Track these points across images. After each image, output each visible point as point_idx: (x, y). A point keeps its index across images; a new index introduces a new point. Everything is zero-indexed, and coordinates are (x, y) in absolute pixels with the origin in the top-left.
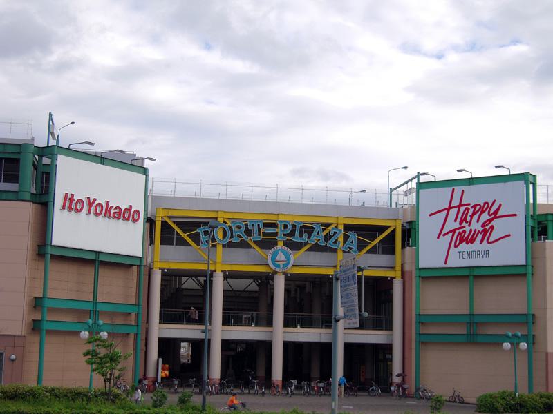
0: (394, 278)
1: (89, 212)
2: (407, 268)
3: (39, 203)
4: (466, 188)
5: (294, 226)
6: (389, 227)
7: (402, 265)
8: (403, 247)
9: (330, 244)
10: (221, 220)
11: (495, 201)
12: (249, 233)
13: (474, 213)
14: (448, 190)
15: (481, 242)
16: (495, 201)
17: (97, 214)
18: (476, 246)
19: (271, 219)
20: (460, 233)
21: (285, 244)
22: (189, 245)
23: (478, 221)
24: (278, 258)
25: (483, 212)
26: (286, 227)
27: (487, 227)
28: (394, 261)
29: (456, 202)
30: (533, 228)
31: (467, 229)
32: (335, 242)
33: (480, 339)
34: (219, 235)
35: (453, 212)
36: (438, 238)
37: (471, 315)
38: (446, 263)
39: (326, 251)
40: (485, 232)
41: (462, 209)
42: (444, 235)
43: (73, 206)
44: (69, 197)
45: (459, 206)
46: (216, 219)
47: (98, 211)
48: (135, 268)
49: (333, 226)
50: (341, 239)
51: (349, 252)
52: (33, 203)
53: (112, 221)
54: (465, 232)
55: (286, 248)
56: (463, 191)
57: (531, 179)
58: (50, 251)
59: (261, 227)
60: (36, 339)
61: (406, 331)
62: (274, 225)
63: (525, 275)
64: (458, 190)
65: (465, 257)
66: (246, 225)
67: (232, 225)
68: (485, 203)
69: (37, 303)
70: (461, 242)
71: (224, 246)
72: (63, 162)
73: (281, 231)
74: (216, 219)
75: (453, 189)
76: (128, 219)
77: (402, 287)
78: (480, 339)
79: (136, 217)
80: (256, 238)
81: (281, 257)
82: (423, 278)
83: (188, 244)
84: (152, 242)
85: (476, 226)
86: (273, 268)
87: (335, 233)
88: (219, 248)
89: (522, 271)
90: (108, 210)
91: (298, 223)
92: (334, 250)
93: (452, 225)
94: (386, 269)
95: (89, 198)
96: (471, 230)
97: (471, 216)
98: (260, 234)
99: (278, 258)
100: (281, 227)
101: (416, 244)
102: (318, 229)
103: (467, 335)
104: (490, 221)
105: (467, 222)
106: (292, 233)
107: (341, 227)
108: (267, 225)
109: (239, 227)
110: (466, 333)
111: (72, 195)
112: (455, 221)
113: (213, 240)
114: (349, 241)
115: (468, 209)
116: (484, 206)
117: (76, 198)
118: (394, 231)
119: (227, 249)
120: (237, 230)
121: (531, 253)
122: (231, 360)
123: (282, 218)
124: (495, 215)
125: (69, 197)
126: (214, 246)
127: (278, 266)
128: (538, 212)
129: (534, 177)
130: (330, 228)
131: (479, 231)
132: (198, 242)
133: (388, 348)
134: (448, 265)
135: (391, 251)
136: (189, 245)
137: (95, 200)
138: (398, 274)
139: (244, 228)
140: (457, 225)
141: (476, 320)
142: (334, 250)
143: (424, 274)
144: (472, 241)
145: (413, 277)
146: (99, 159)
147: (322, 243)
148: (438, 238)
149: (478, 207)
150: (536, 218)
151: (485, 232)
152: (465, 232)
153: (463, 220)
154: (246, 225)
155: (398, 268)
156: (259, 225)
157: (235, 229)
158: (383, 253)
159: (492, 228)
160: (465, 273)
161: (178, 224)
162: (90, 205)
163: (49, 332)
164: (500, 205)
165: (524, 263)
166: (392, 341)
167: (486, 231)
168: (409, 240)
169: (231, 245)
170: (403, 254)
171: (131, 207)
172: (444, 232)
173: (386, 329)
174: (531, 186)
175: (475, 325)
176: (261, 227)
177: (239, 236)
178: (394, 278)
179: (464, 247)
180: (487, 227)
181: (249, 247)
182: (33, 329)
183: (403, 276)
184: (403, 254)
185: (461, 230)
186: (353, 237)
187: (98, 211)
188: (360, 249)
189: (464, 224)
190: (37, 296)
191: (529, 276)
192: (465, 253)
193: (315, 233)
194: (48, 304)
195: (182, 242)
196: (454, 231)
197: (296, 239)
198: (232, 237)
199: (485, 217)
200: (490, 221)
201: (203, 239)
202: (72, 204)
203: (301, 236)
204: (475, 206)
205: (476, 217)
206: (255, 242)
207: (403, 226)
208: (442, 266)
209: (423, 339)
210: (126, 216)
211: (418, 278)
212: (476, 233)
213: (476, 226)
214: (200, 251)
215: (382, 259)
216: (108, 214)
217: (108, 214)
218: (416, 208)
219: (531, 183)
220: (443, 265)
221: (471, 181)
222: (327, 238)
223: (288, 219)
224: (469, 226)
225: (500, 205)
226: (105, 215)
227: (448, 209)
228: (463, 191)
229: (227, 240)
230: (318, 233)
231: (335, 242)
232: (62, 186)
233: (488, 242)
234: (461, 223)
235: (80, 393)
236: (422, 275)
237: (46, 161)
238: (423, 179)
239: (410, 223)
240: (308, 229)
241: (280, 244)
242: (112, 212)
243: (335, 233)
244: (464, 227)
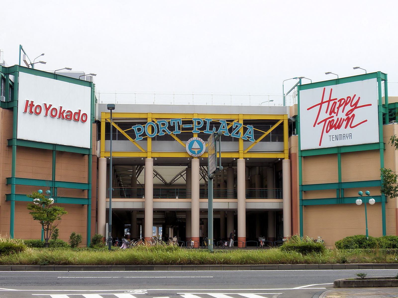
0: (284, 159)
1: (46, 115)
2: (293, 151)
3: (8, 109)
4: (333, 87)
5: (205, 123)
6: (278, 120)
7: (290, 150)
8: (290, 134)
9: (233, 135)
10: (149, 120)
11: (355, 95)
12: (171, 128)
13: (340, 106)
14: (321, 89)
15: (346, 128)
16: (355, 95)
17: (53, 116)
18: (342, 130)
19: (189, 117)
20: (330, 122)
21: (199, 136)
22: (127, 139)
23: (343, 112)
24: (193, 147)
25: (346, 104)
26: (199, 123)
27: (350, 116)
28: (283, 147)
29: (326, 98)
30: (384, 115)
31: (335, 118)
32: (237, 133)
33: (346, 201)
34: (149, 131)
35: (325, 106)
36: (314, 126)
37: (340, 183)
38: (320, 145)
39: (232, 141)
40: (348, 119)
41: (332, 103)
42: (318, 124)
44: (30, 103)
45: (330, 100)
46: (147, 119)
47: (54, 114)
48: (86, 156)
49: (236, 121)
50: (241, 131)
51: (248, 140)
52: (3, 108)
53: (65, 122)
54: (333, 120)
55: (200, 139)
56: (332, 89)
57: (382, 77)
58: (15, 143)
59: (181, 124)
61: (293, 199)
62: (191, 122)
63: (378, 151)
64: (328, 88)
65: (334, 139)
66: (169, 123)
67: (159, 123)
68: (348, 98)
69: (9, 181)
70: (331, 128)
71: (153, 139)
72: (23, 77)
73: (196, 126)
74: (147, 119)
75: (325, 88)
76: (78, 120)
77: (290, 166)
78: (346, 201)
79: (84, 119)
80: (177, 132)
81: (196, 146)
82: (304, 157)
83: (127, 139)
84: (99, 138)
85: (342, 115)
86: (190, 154)
87: (237, 126)
88: (149, 141)
89: (376, 147)
90: (61, 114)
91: (208, 120)
92: (237, 140)
93: (324, 115)
94: (281, 153)
95: (45, 105)
96: (338, 119)
97: (338, 108)
98: (179, 129)
99: (193, 147)
100: (195, 123)
101: (298, 133)
102: (223, 124)
103: (337, 198)
104: (352, 110)
105: (335, 113)
106: (204, 128)
107: (241, 122)
108: (185, 122)
109: (163, 124)
110: (336, 197)
112: (326, 112)
113: (144, 134)
114: (248, 132)
115: (335, 103)
116: (347, 100)
117: (35, 104)
118: (282, 124)
119: (156, 142)
120: (162, 126)
121: (382, 133)
123: (196, 117)
124: (356, 106)
125: (30, 103)
126: (146, 139)
127: (194, 153)
128: (389, 102)
129: (385, 75)
130: (233, 123)
131: (344, 119)
132: (133, 137)
133: (279, 213)
134: (322, 146)
135: (281, 139)
136: (127, 139)
137: (50, 106)
138: (286, 155)
139: (167, 125)
140: (328, 116)
141: (344, 186)
142: (237, 140)
144: (339, 127)
145: (298, 157)
146: (53, 76)
147: (227, 134)
148: (314, 126)
149: (343, 101)
150: (387, 106)
151: (348, 119)
152: (333, 120)
153: (332, 111)
154: (169, 123)
155: (287, 152)
156: (178, 122)
157: (161, 126)
158: (279, 141)
159: (353, 116)
160: (335, 151)
161: (120, 124)
162: (47, 109)
163: (18, 204)
164: (359, 98)
165: (378, 142)
166: (283, 207)
167: (349, 119)
168: (294, 131)
169: (159, 138)
170: (290, 141)
171: (80, 111)
172: (318, 122)
173: (279, 198)
174: (383, 82)
175: (342, 190)
176: (181, 124)
177: (164, 131)
178: (284, 159)
179: (333, 132)
180: (350, 116)
181: (173, 139)
182: (6, 201)
183: (290, 157)
184: (290, 141)
185: (331, 119)
186: (251, 128)
187: (54, 114)
188: (256, 138)
189: (333, 114)
190: (8, 177)
191: (382, 151)
192: (334, 137)
193: (221, 127)
194: (14, 182)
195: (122, 137)
196: (325, 120)
197: (206, 132)
198: (158, 132)
199: (348, 108)
200: (352, 110)
201: (137, 134)
203: (211, 129)
204: (340, 100)
206: (177, 136)
207: (289, 120)
209: (305, 203)
210: (76, 118)
211: (300, 157)
212: (342, 120)
213: (342, 115)
214: (136, 143)
215: (274, 146)
216: (61, 117)
217: (61, 117)
218: (298, 106)
219: (382, 80)
220: (317, 147)
221: (337, 81)
222: (231, 130)
223: (201, 117)
224: (337, 115)
225: (359, 98)
226: (59, 117)
227: (321, 104)
228: (332, 89)
229: (155, 134)
230: (224, 127)
231: (237, 133)
233: (351, 127)
234: (330, 114)
235: (43, 247)
236: (303, 155)
237: (11, 77)
238: (304, 82)
239: (295, 117)
240: (216, 124)
241: (195, 137)
242: (65, 115)
243: (237, 126)
244: (333, 117)
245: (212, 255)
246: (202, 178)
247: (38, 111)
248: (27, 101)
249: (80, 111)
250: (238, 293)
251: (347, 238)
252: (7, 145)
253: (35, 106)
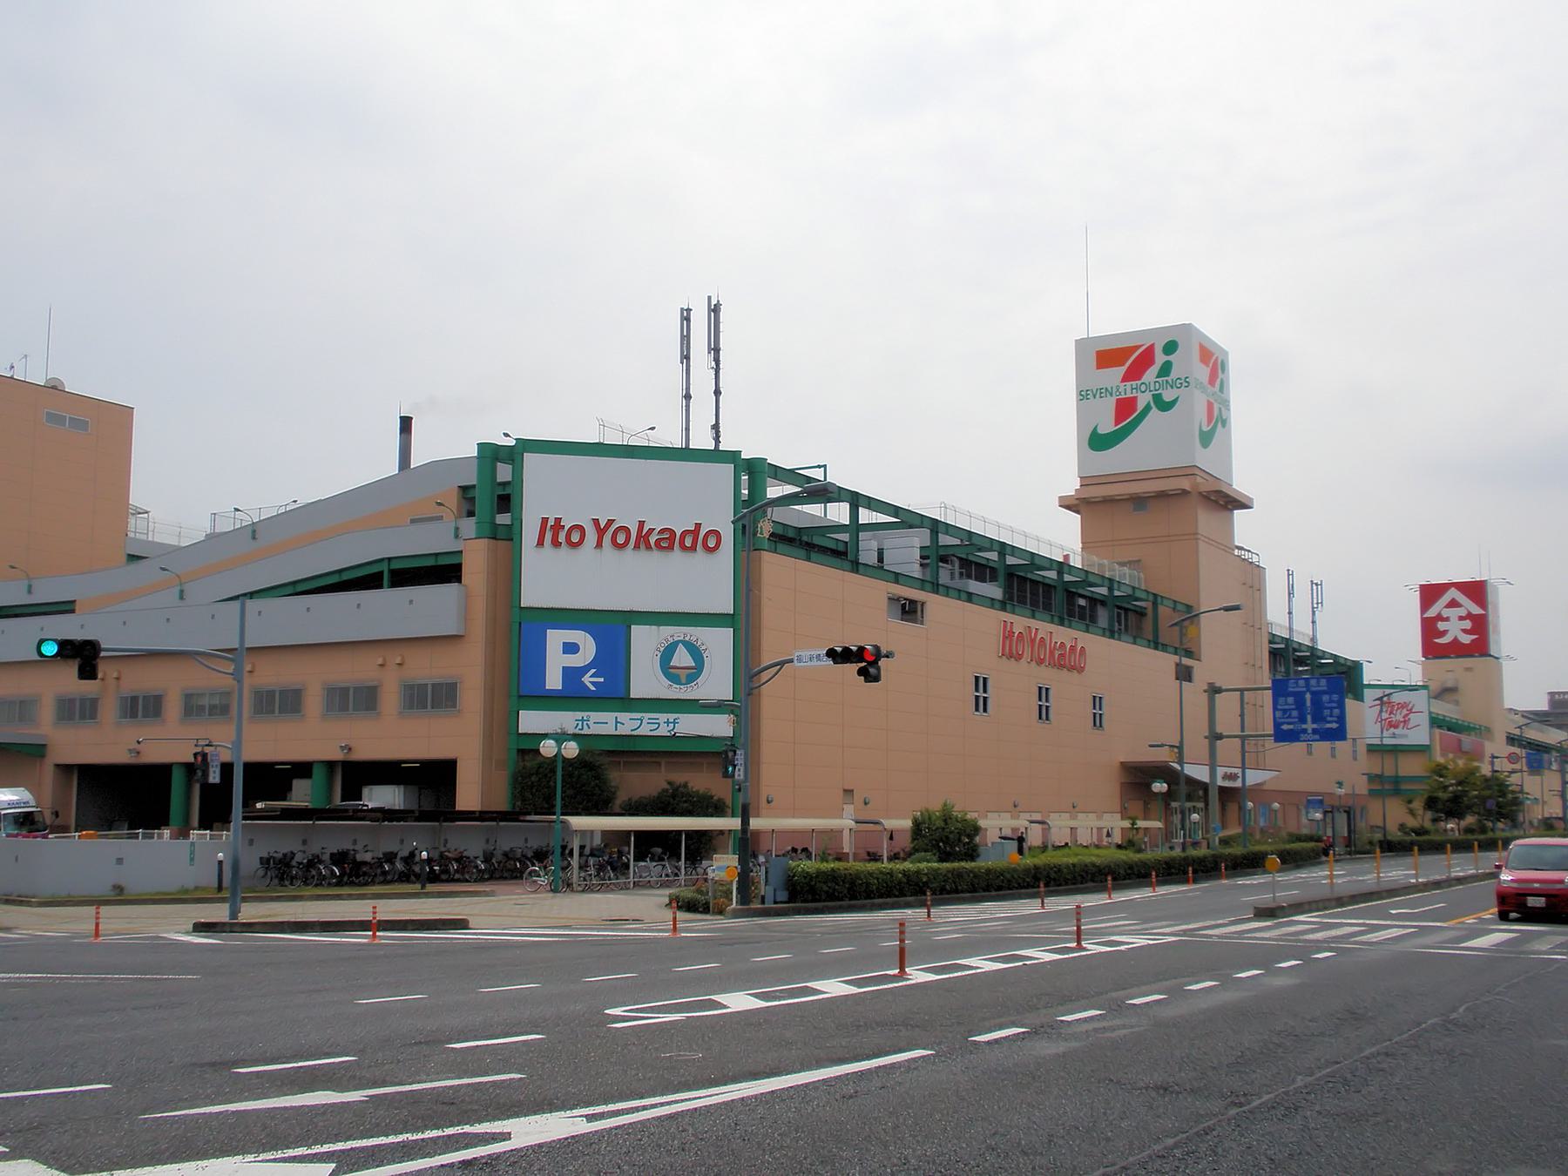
1: (599, 545)
13: (1398, 708)
18: (1397, 731)
43: (562, 538)
47: (621, 539)
53: (656, 555)
60: (898, 926)
76: (693, 548)
79: (711, 544)
85: (1399, 717)
95: (596, 522)
98: (1208, 848)
104: (1407, 715)
111: (558, 520)
122: (1320, 798)
124: (1411, 711)
125: (551, 523)
143: (1371, 748)
159: (1409, 719)
162: (601, 532)
171: (698, 526)
199: (1405, 712)
200: (1407, 715)
202: (555, 533)
205: (1399, 711)
208: (628, 734)
213: (1399, 717)
226: (637, 546)
232: (534, 510)
245: (1139, 856)
246: (1181, 684)
247: (575, 538)
248: (545, 520)
249: (698, 526)
250: (1292, 916)
251: (641, 797)
252: (1207, 734)
253: (566, 528)
